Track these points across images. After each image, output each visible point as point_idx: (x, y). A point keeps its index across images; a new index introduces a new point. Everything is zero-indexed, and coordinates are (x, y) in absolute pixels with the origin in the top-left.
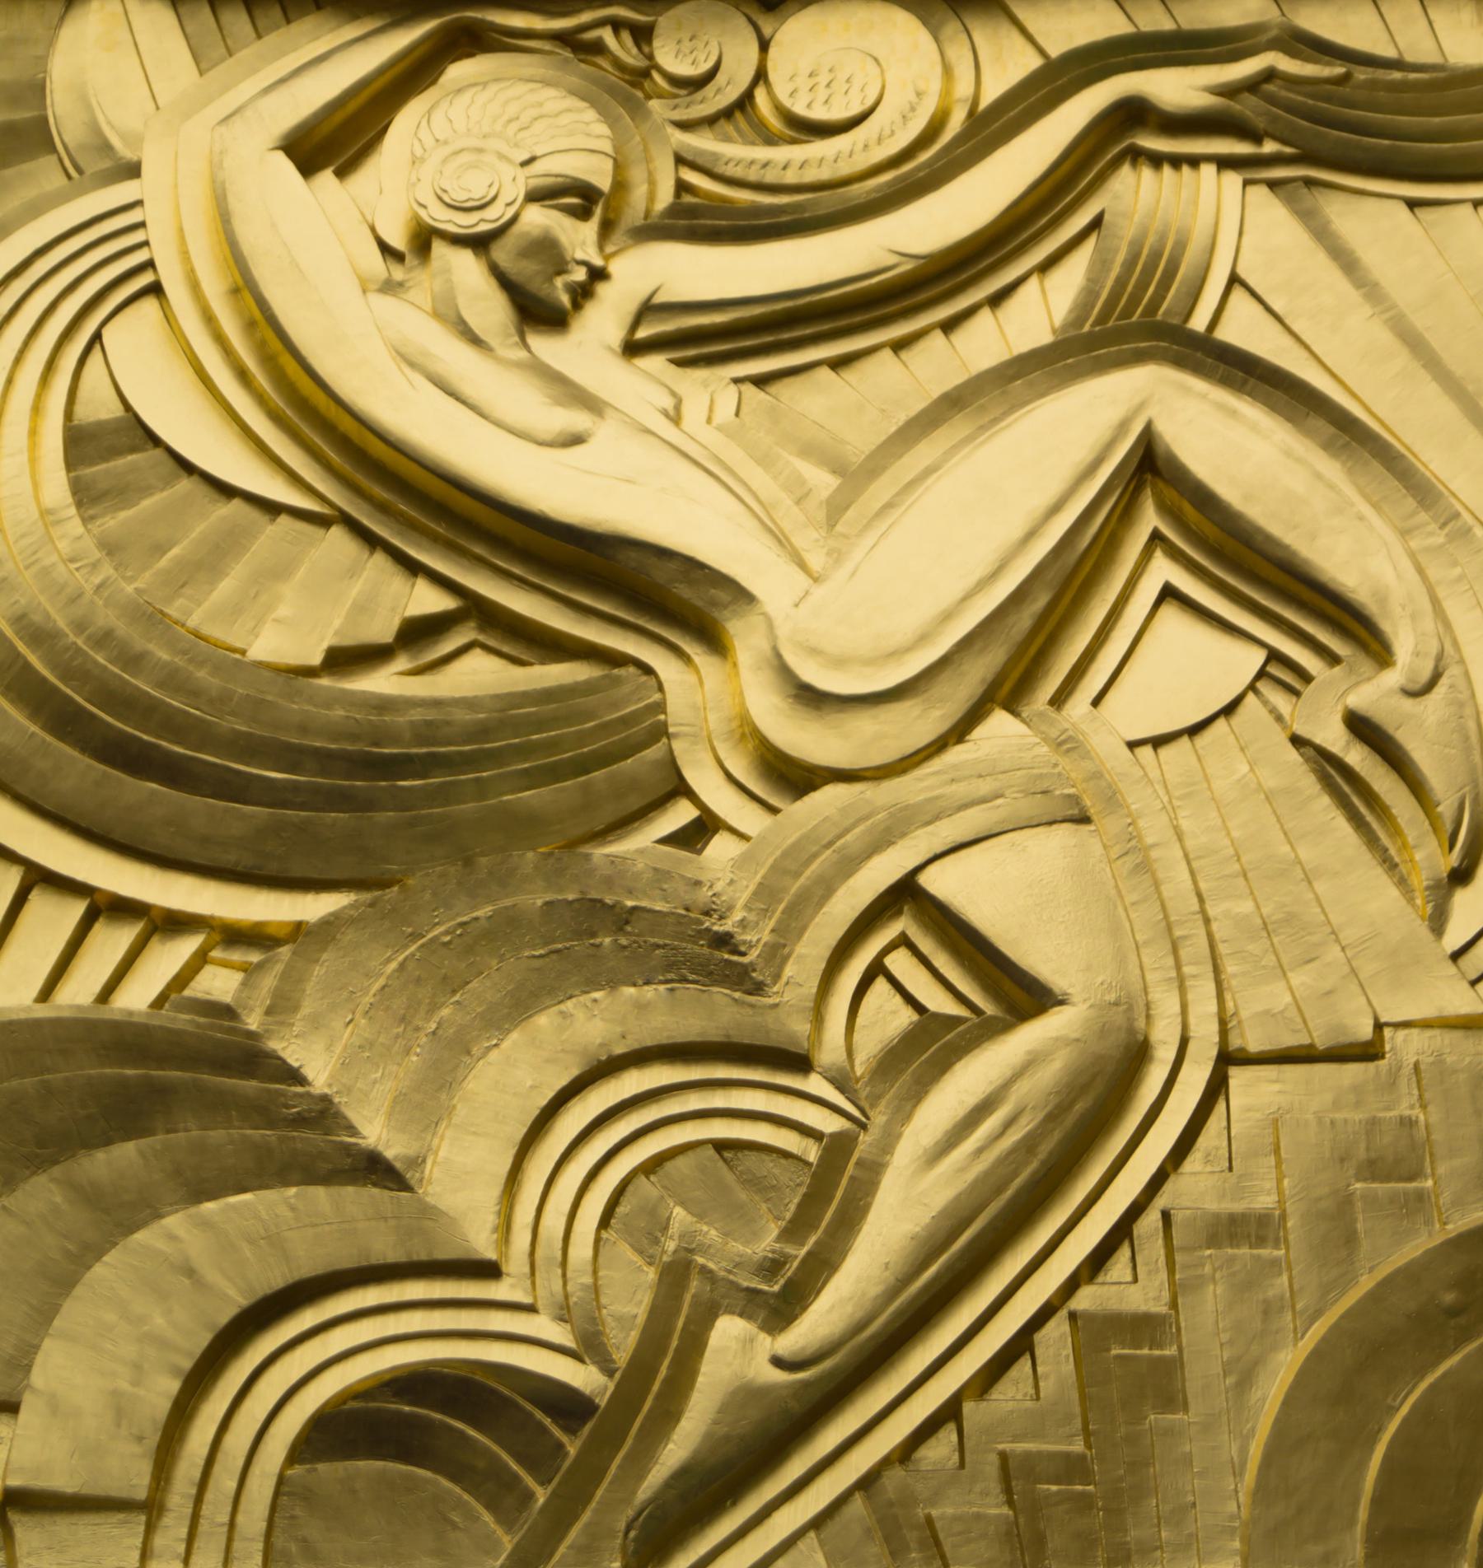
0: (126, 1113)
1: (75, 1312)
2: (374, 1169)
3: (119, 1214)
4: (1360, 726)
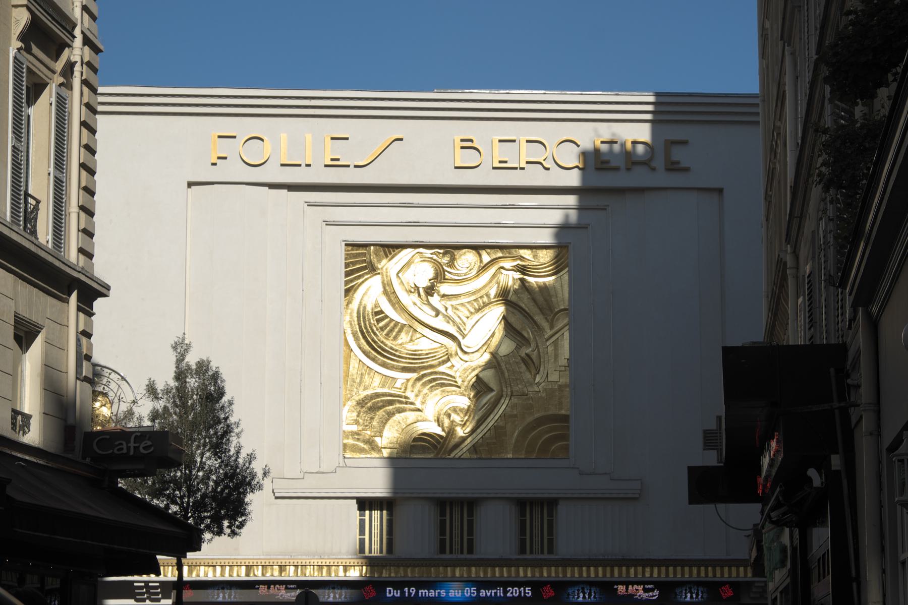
1: (387, 427)
2: (419, 410)
3: (391, 415)
4: (527, 354)
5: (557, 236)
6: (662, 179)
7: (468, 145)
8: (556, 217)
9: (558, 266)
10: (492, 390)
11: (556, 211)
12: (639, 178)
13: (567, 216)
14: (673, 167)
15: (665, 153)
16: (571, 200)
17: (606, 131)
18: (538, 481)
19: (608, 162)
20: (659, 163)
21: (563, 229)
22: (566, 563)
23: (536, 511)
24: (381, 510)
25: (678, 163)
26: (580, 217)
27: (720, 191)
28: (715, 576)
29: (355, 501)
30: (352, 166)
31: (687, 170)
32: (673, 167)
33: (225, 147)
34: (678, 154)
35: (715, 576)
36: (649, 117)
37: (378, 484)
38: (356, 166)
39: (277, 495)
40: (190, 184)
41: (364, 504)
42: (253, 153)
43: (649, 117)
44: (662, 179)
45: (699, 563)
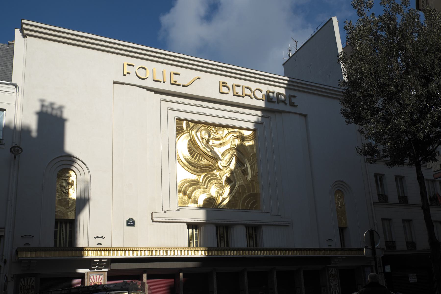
0: (194, 185)
3: (195, 189)
5: (255, 126)
6: (288, 108)
7: (224, 85)
8: (254, 119)
9: (255, 137)
10: (232, 182)
11: (254, 117)
12: (281, 107)
13: (258, 119)
14: (292, 105)
15: (290, 100)
16: (259, 113)
17: (271, 89)
18: (252, 217)
19: (272, 99)
20: (287, 102)
21: (257, 123)
22: (266, 249)
23: (253, 230)
24: (193, 230)
25: (294, 103)
26: (262, 119)
27: (305, 116)
28: (188, 254)
29: (186, 224)
30: (181, 86)
31: (296, 106)
32: (292, 105)
33: (127, 69)
34: (293, 100)
35: (188, 254)
36: (285, 86)
37: (200, 216)
38: (183, 86)
39: (154, 220)
40: (115, 83)
41: (191, 226)
42: (141, 73)
43: (285, 86)
44: (288, 108)
45: (295, 249)
